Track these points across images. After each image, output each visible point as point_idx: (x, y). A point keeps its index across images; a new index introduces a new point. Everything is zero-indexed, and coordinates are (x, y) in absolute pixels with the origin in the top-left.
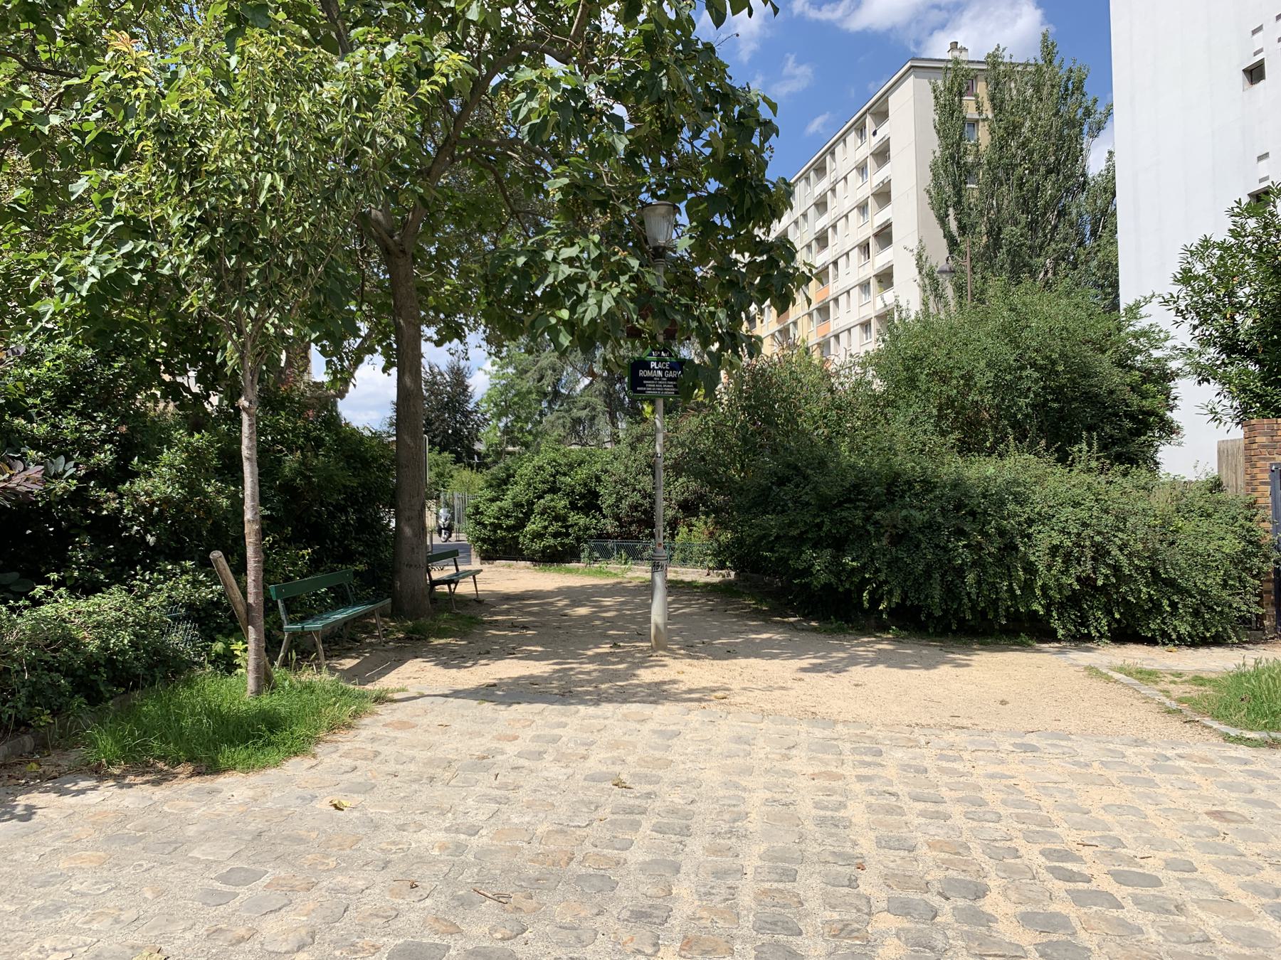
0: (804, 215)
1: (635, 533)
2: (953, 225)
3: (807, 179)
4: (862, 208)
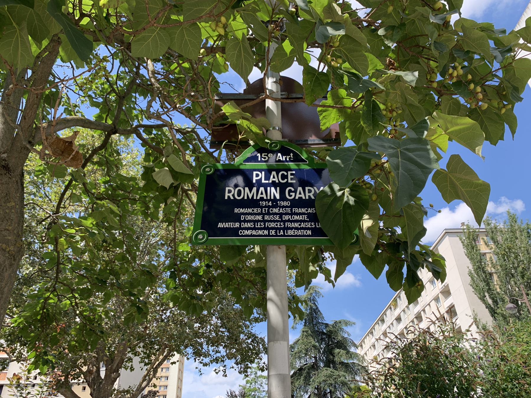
0: (392, 324)
1: (342, 363)
2: (490, 301)
3: (391, 308)
4: (437, 299)
